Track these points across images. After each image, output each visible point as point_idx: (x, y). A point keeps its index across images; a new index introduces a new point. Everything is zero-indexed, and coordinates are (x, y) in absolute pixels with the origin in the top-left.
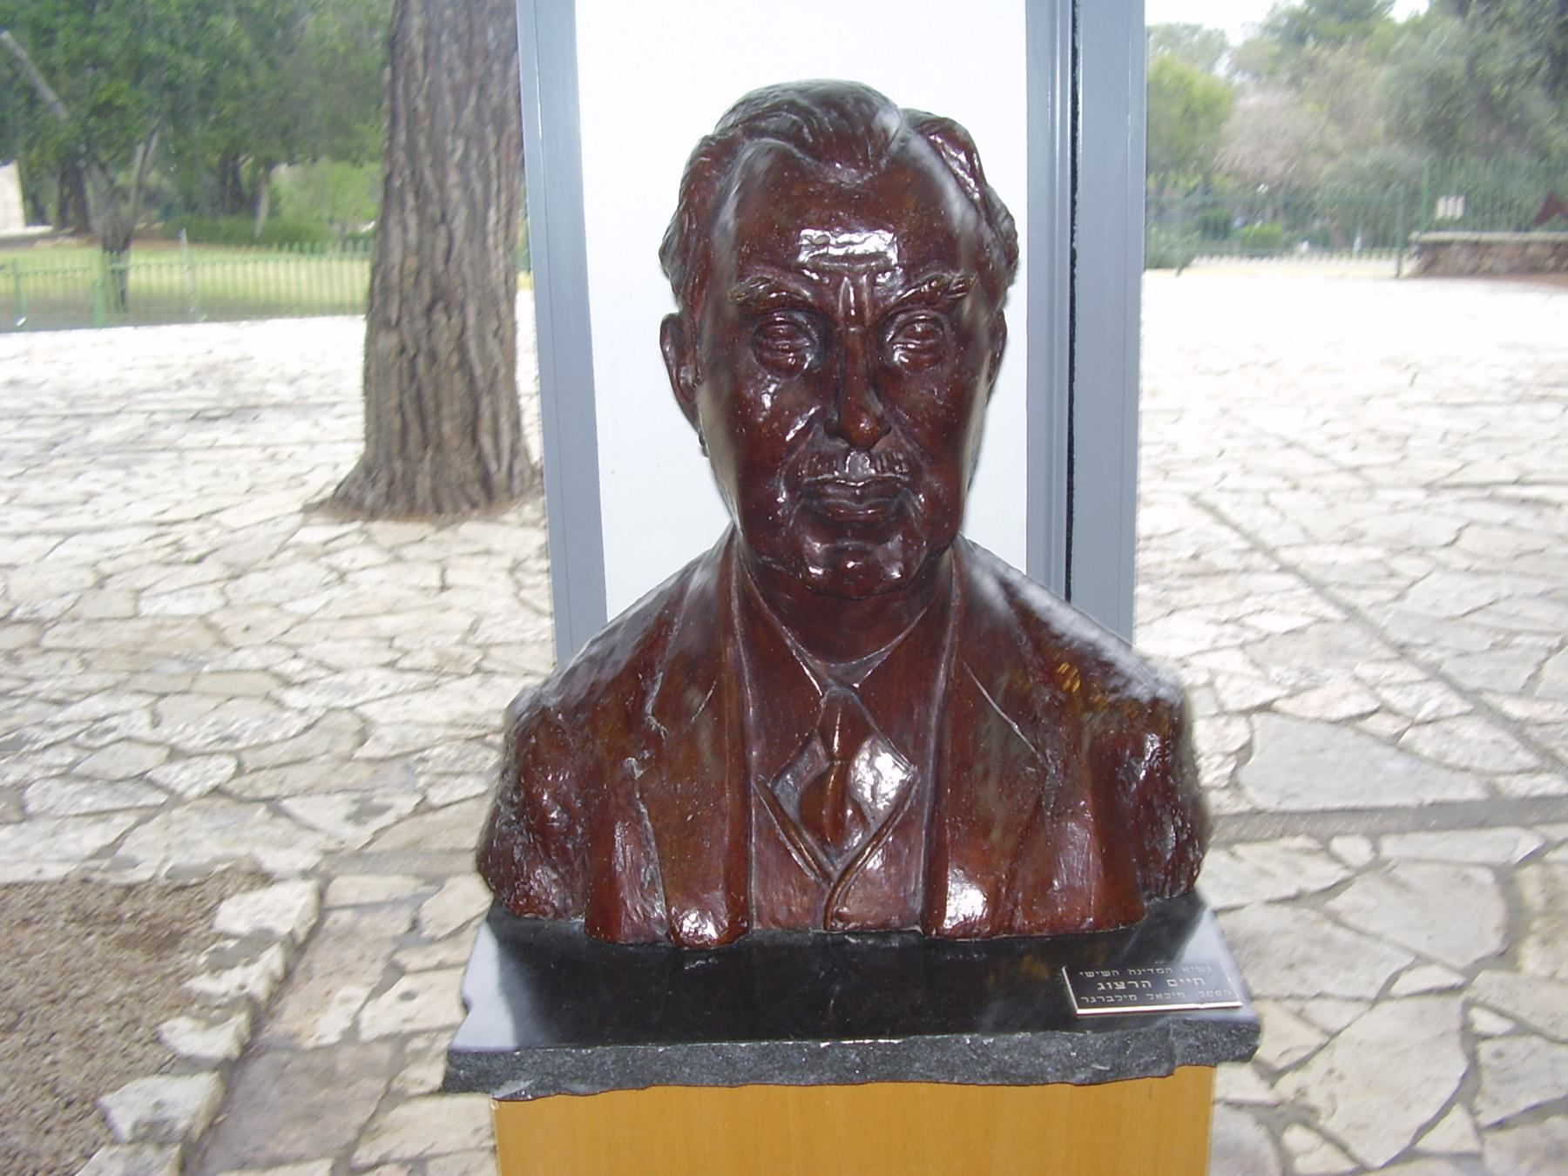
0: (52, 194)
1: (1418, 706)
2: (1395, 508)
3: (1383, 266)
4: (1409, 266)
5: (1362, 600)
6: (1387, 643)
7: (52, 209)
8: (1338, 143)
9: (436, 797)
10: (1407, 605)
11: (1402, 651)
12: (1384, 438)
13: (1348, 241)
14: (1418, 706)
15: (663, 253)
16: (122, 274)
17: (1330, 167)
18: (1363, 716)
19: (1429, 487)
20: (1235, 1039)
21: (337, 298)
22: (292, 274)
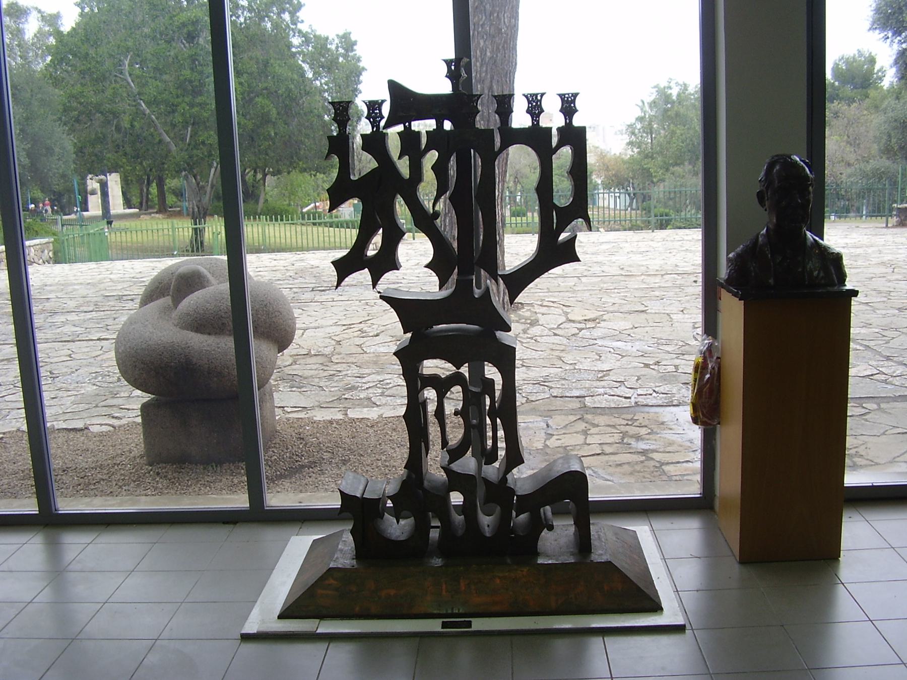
0: (135, 191)
1: (894, 372)
2: (884, 316)
3: (880, 222)
4: (893, 220)
5: (871, 344)
6: (882, 356)
7: (135, 200)
8: (852, 158)
9: (531, 398)
10: (890, 345)
11: (888, 358)
12: (880, 292)
13: (858, 210)
14: (894, 372)
15: (761, 197)
16: (202, 231)
17: (849, 170)
18: (872, 375)
19: (899, 309)
20: (855, 293)
21: (278, 245)
22: (267, 231)
